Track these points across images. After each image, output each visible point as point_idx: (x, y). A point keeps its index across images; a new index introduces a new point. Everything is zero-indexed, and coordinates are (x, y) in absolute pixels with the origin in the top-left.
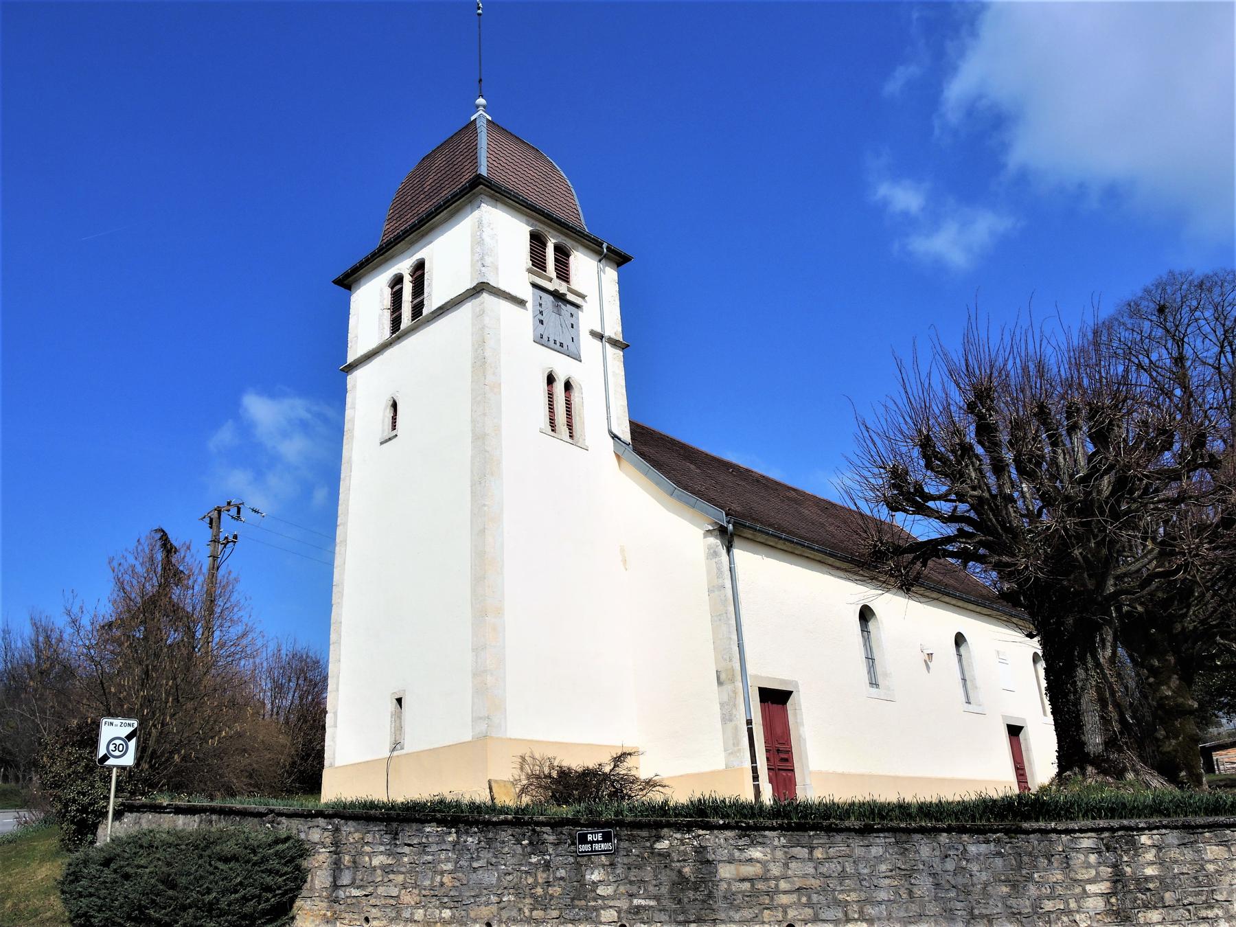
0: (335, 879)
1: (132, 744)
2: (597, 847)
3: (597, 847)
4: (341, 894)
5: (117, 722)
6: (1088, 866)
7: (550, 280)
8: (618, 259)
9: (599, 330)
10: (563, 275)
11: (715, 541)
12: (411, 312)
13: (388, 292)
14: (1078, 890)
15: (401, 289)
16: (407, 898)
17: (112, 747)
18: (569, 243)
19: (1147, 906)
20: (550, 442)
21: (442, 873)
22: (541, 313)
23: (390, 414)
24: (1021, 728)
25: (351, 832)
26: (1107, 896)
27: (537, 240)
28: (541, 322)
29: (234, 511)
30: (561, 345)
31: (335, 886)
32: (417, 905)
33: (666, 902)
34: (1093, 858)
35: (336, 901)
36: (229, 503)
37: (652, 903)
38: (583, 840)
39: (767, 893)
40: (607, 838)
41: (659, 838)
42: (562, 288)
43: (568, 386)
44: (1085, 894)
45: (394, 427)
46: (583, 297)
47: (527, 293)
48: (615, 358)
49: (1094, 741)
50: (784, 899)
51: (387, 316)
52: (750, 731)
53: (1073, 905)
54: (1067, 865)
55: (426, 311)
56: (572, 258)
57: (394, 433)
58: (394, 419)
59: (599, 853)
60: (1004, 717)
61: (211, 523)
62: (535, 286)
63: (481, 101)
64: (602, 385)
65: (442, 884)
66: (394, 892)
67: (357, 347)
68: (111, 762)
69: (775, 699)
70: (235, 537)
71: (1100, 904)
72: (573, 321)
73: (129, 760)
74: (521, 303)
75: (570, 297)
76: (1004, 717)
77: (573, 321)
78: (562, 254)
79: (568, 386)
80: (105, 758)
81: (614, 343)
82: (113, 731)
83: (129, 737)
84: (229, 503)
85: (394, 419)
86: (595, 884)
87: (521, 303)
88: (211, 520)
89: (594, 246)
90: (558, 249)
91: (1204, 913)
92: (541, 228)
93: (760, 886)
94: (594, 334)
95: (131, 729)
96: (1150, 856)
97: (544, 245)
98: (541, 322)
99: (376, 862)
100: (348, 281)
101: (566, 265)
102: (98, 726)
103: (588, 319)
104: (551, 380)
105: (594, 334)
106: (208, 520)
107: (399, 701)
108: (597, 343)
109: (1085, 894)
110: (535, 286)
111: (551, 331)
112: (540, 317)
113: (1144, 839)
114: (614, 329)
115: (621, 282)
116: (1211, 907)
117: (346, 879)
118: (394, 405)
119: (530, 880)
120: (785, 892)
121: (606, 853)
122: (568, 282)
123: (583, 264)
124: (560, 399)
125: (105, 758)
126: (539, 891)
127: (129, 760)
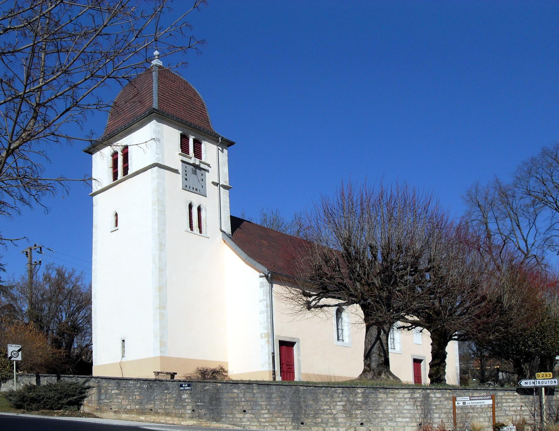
0: (99, 397)
1: (20, 353)
2: (186, 388)
3: (186, 388)
4: (102, 402)
5: (14, 345)
6: (339, 397)
7: (191, 158)
8: (226, 144)
9: (217, 181)
10: (198, 154)
11: (264, 280)
12: (121, 168)
13: (110, 159)
14: (334, 404)
15: (117, 158)
16: (124, 403)
17: (13, 354)
18: (199, 137)
19: (356, 409)
20: (190, 235)
21: (135, 395)
22: (186, 175)
23: (114, 219)
24: (420, 361)
25: (104, 383)
26: (344, 406)
27: (184, 139)
28: (186, 179)
29: (39, 250)
30: (196, 190)
31: (99, 399)
32: (128, 405)
33: (207, 404)
34: (341, 395)
35: (100, 404)
36: (35, 245)
37: (202, 404)
38: (181, 386)
39: (238, 402)
40: (189, 386)
41: (206, 386)
42: (197, 162)
43: (199, 209)
44: (336, 405)
45: (117, 226)
46: (209, 165)
47: (179, 166)
48: (225, 194)
49: (374, 365)
50: (243, 403)
51: (111, 171)
52: (273, 357)
53: (332, 408)
54: (332, 397)
55: (130, 172)
56: (203, 145)
57: (117, 228)
58: (117, 221)
59: (186, 390)
60: (412, 355)
61: (27, 254)
62: (183, 161)
63: (156, 53)
64: (217, 209)
65: (136, 398)
66: (120, 401)
67: (96, 187)
68: (12, 359)
69: (286, 346)
70: (40, 262)
71: (341, 408)
72: (202, 177)
73: (19, 358)
74: (176, 171)
75: (202, 166)
76: (412, 355)
77: (202, 177)
78: (197, 144)
79: (199, 209)
80: (11, 357)
81: (225, 187)
82: (12, 349)
83: (19, 351)
84: (35, 245)
85: (117, 221)
86: (185, 399)
87: (176, 171)
88: (27, 252)
89: (214, 138)
90: (195, 141)
91: (375, 412)
92: (186, 131)
93: (236, 400)
94: (214, 183)
95: (19, 348)
96: (360, 395)
97: (188, 139)
98: (186, 179)
99: (113, 392)
100: (90, 152)
101: (200, 148)
102: (415, 382)
103: (211, 177)
104: (190, 206)
105: (214, 183)
106: (25, 253)
107: (124, 341)
108: (216, 188)
109: (336, 405)
110: (183, 161)
111: (191, 183)
112: (186, 177)
113: (359, 391)
114: (225, 181)
115: (229, 156)
116: (377, 410)
117: (103, 397)
118: (116, 215)
119: (164, 397)
120: (243, 401)
121: (188, 390)
122: (201, 159)
123: (209, 150)
124: (195, 219)
125: (11, 357)
126: (167, 400)
127: (19, 358)
